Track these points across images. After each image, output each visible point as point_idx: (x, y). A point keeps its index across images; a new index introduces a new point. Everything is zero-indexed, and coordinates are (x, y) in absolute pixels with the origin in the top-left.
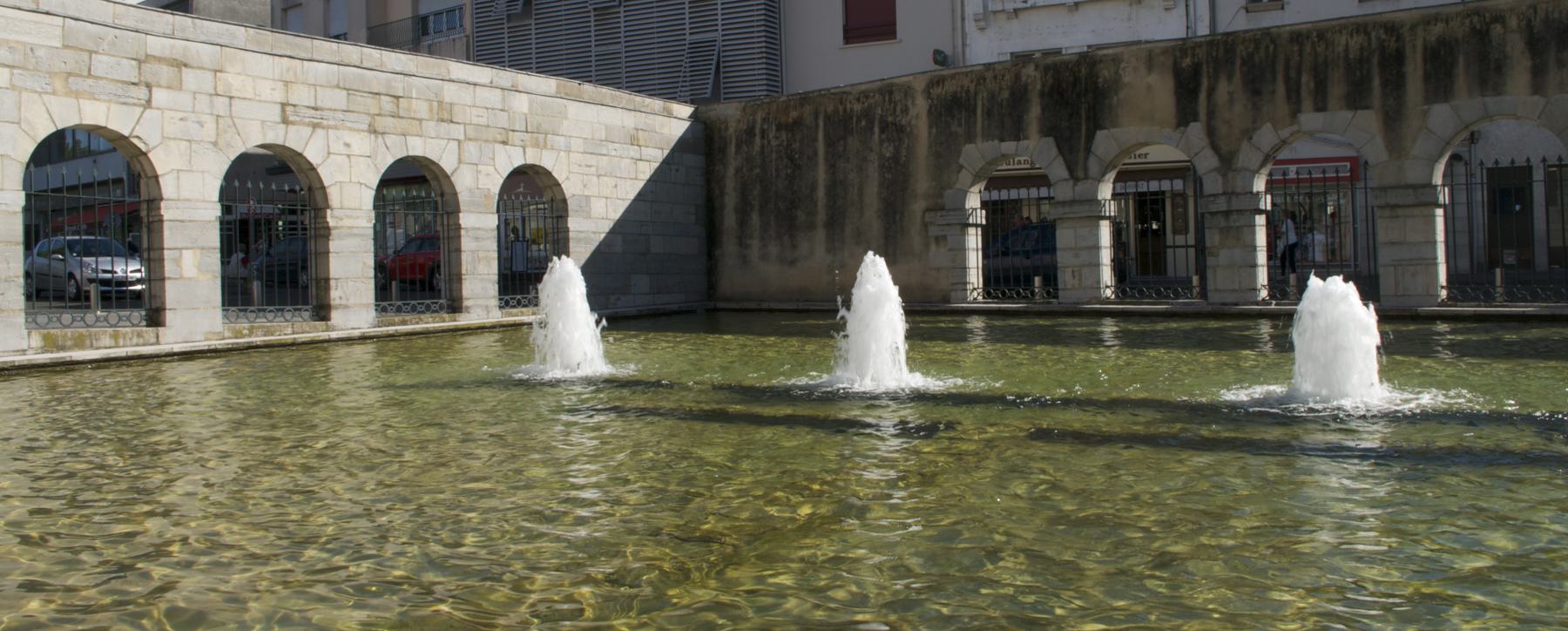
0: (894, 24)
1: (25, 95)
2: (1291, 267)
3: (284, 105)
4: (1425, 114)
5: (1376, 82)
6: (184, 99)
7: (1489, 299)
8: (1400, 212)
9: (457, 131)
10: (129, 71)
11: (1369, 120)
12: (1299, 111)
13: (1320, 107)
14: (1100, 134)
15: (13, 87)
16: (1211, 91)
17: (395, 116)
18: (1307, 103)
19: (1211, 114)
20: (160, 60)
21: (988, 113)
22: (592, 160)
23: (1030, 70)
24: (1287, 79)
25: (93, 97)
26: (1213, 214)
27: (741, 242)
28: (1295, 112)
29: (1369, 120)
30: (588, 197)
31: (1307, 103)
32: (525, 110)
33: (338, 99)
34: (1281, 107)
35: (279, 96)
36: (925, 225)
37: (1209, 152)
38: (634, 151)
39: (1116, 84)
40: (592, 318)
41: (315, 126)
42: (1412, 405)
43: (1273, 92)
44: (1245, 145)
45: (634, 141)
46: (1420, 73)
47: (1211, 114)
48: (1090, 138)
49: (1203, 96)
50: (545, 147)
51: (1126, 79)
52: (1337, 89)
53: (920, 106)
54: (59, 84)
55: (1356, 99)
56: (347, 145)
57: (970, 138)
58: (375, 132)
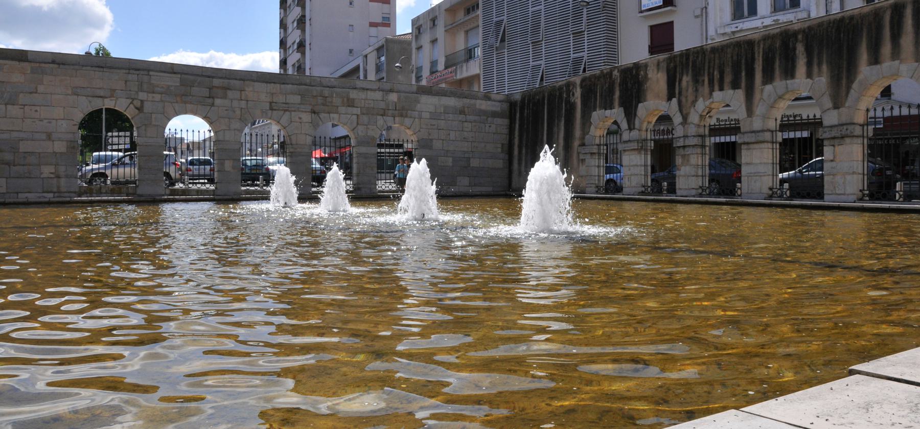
0: (673, 44)
1: (166, 104)
2: (326, 162)
3: (271, 103)
4: (762, 90)
5: (743, 74)
6: (226, 102)
7: (893, 199)
8: (752, 146)
9: (357, 111)
10: (206, 92)
11: (740, 94)
12: (713, 91)
13: (721, 89)
14: (640, 105)
15: (162, 101)
16: (680, 80)
17: (323, 105)
18: (716, 87)
19: (680, 93)
20: (217, 87)
21: (601, 96)
22: (434, 122)
23: (616, 73)
24: (709, 75)
25: (191, 103)
26: (679, 147)
27: (520, 164)
28: (712, 91)
29: (740, 94)
30: (431, 140)
31: (716, 87)
32: (396, 100)
33: (297, 99)
34: (706, 89)
35: (269, 100)
36: (578, 153)
37: (679, 114)
38: (462, 117)
39: (646, 77)
40: (523, 205)
41: (285, 111)
42: (370, 210)
43: (703, 81)
44: (692, 110)
45: (462, 112)
46: (761, 68)
47: (680, 93)
48: (636, 107)
49: (677, 84)
50: (406, 116)
51: (650, 76)
52: (728, 79)
53: (578, 92)
54: (178, 99)
55: (735, 86)
56: (300, 118)
57: (595, 110)
58: (314, 113)
